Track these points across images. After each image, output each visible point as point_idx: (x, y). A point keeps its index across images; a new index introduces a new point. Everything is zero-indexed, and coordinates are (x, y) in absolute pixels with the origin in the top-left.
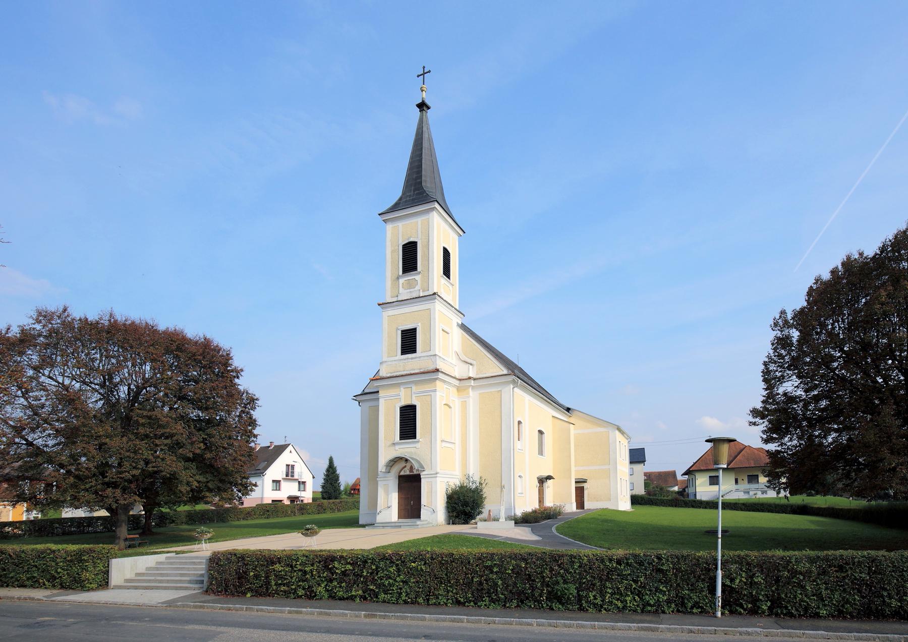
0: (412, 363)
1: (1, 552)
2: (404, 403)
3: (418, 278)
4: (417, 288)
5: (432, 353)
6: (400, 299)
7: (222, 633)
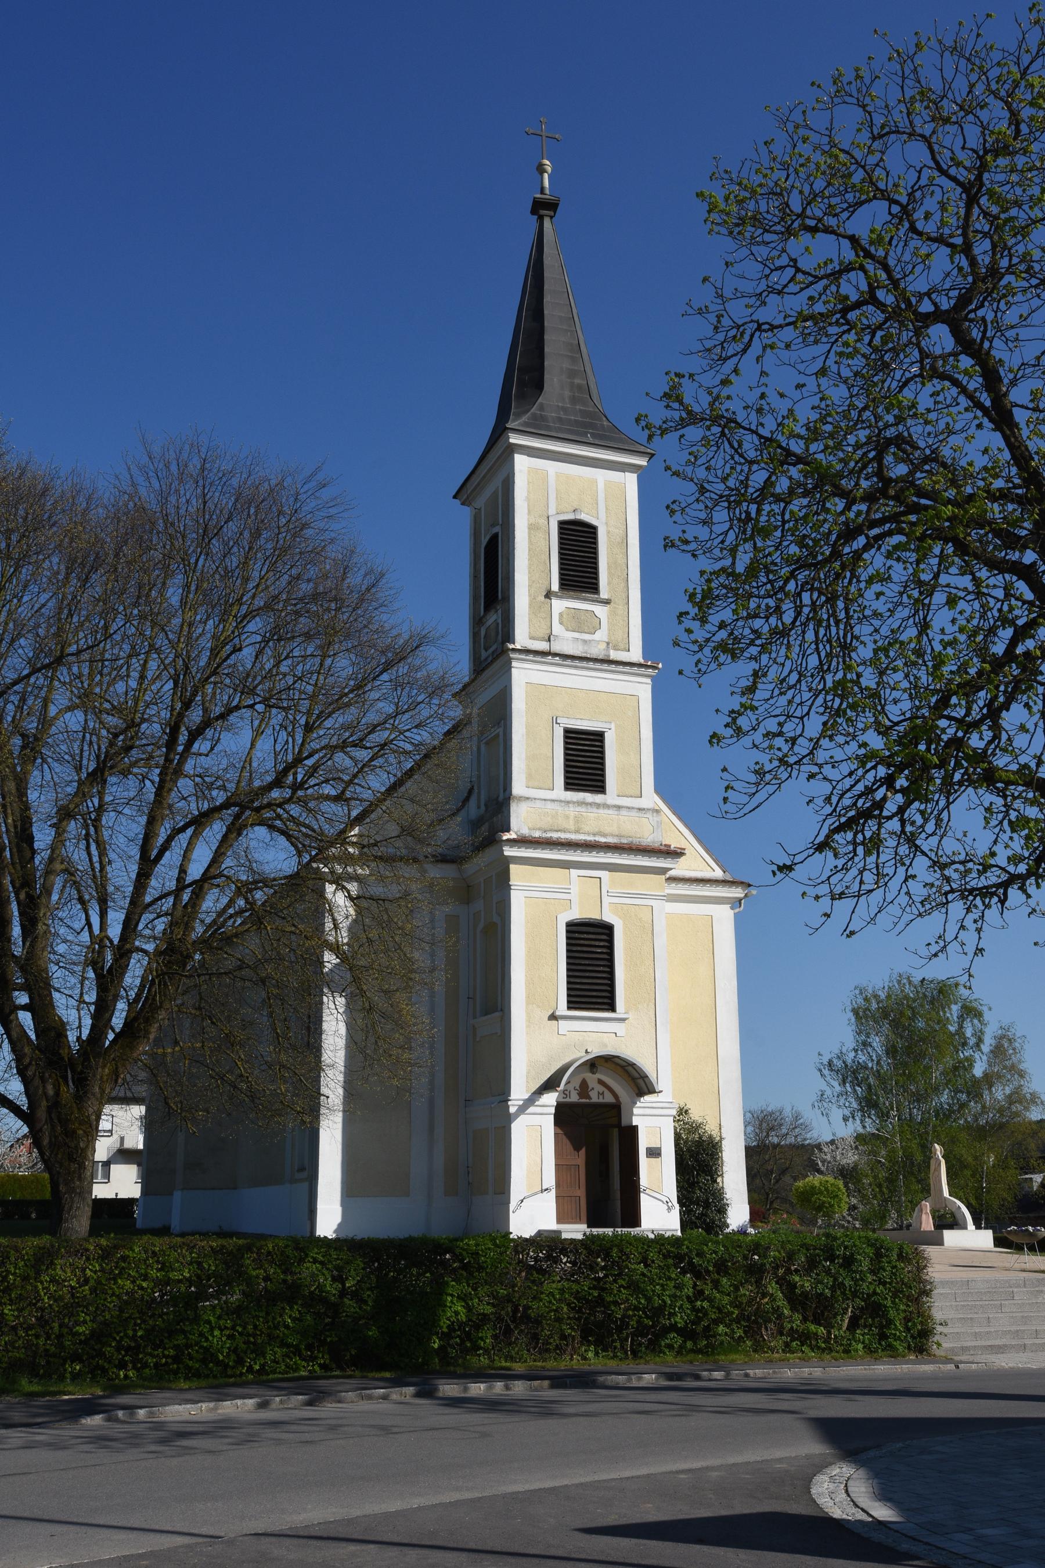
2: (576, 914)
3: (600, 610)
6: (556, 647)
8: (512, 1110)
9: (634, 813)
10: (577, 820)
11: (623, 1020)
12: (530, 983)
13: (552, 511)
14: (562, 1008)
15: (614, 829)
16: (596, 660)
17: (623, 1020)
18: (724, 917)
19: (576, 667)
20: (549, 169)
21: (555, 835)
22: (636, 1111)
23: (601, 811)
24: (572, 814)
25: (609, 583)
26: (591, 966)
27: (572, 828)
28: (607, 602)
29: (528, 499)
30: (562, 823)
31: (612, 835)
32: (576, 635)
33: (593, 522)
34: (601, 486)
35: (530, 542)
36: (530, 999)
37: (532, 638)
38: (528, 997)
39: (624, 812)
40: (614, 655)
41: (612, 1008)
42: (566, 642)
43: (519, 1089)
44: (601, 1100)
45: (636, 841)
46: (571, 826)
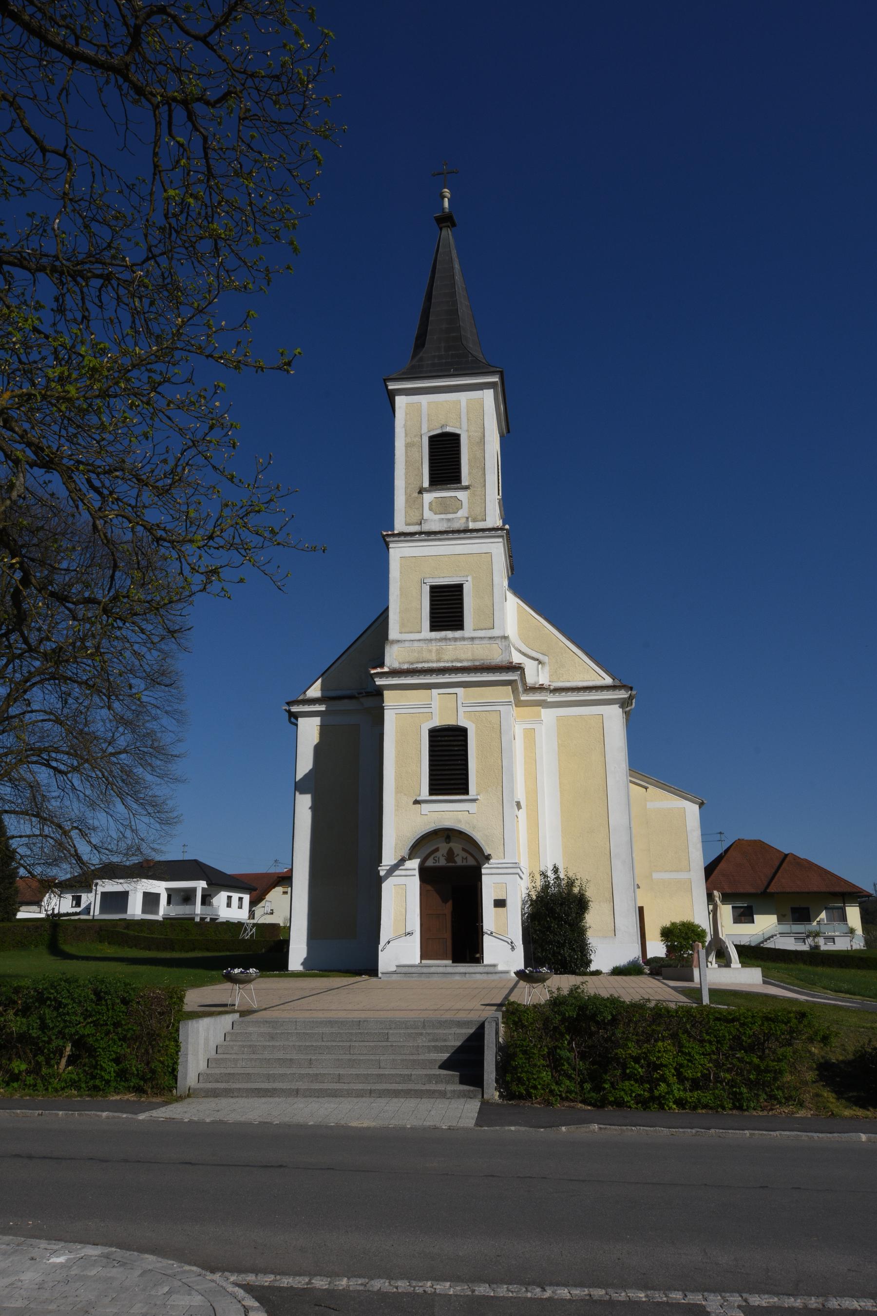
0: (453, 648)
1: (872, 1296)
2: (437, 722)
3: (461, 495)
4: (460, 514)
5: (496, 633)
6: (426, 528)
7: (429, 1041)
8: (382, 873)
9: (486, 641)
10: (438, 652)
11: (474, 800)
12: (398, 777)
13: (424, 430)
14: (425, 793)
15: (469, 655)
16: (459, 531)
17: (474, 800)
18: (613, 718)
19: (440, 540)
20: (448, 195)
21: (420, 666)
22: (483, 871)
23: (458, 643)
24: (434, 648)
25: (470, 473)
26: (448, 762)
27: (434, 658)
28: (467, 488)
29: (405, 426)
30: (426, 655)
31: (468, 660)
32: (443, 516)
33: (457, 431)
34: (464, 404)
35: (407, 456)
36: (399, 790)
37: (407, 524)
38: (397, 788)
39: (477, 642)
40: (471, 526)
41: (466, 791)
42: (434, 522)
43: (389, 858)
44: (465, 863)
45: (487, 662)
46: (434, 657)
